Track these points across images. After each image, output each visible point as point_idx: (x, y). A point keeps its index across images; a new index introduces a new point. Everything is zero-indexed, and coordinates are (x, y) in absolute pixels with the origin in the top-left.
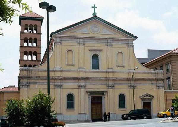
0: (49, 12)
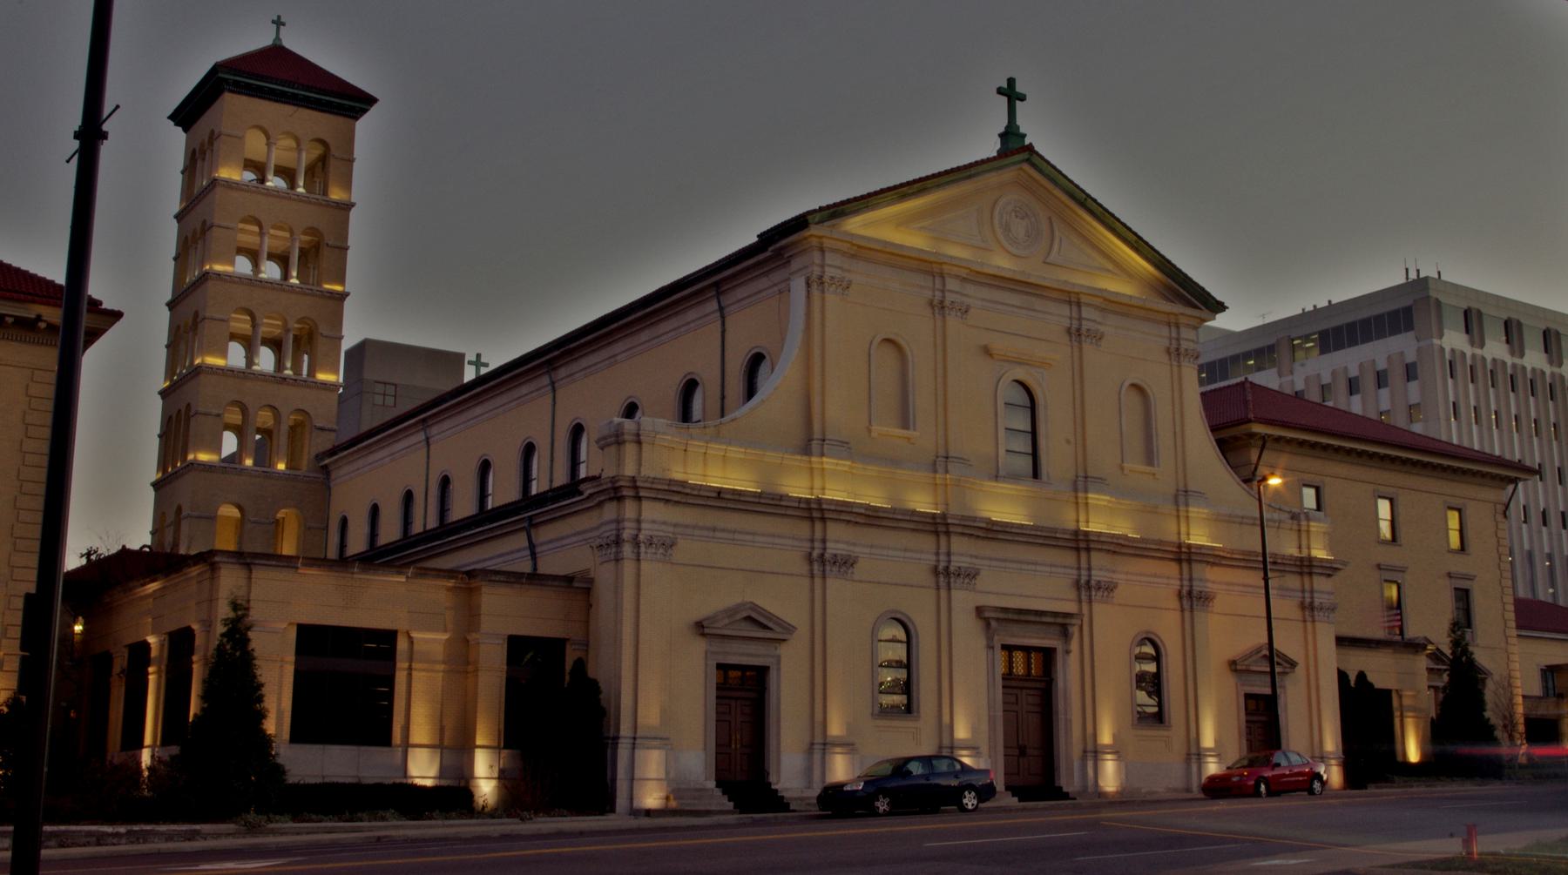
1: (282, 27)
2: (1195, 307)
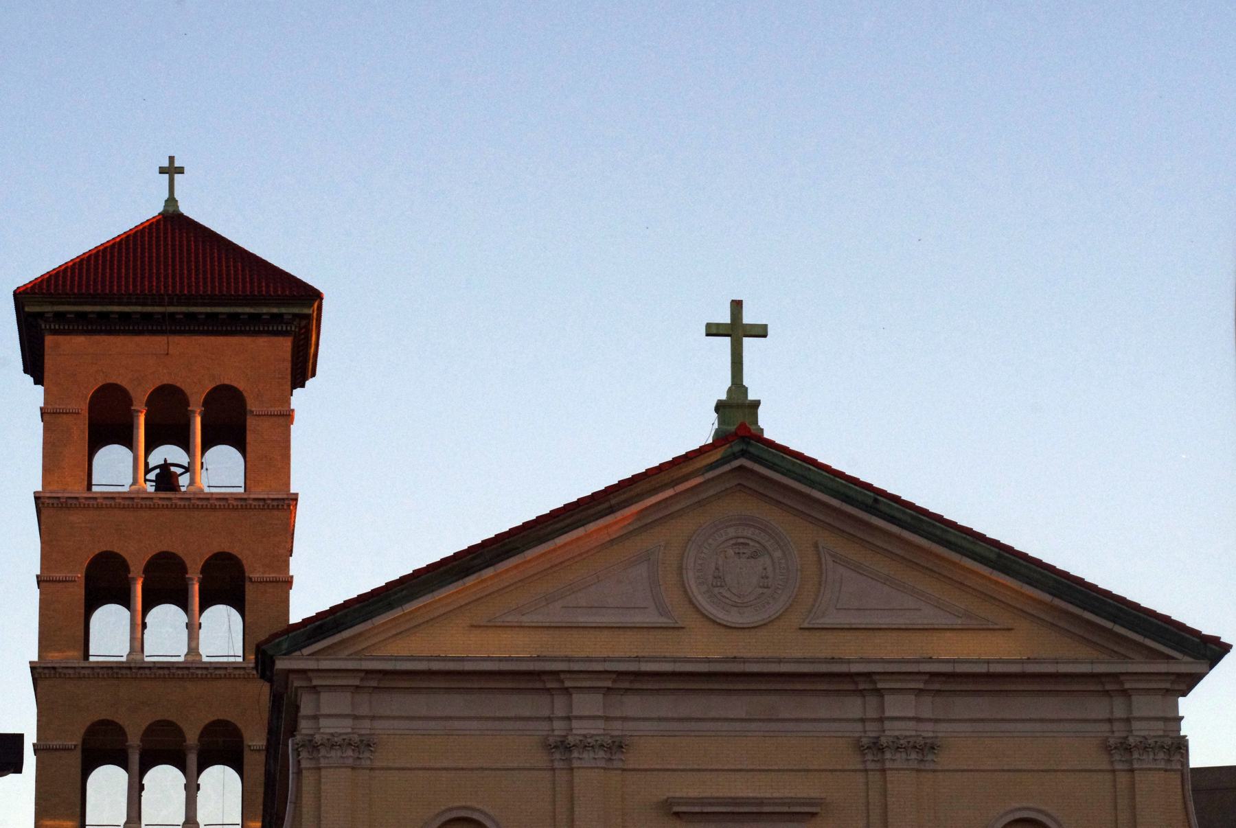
0: (150, 467)
1: (177, 176)
2: (1169, 658)
